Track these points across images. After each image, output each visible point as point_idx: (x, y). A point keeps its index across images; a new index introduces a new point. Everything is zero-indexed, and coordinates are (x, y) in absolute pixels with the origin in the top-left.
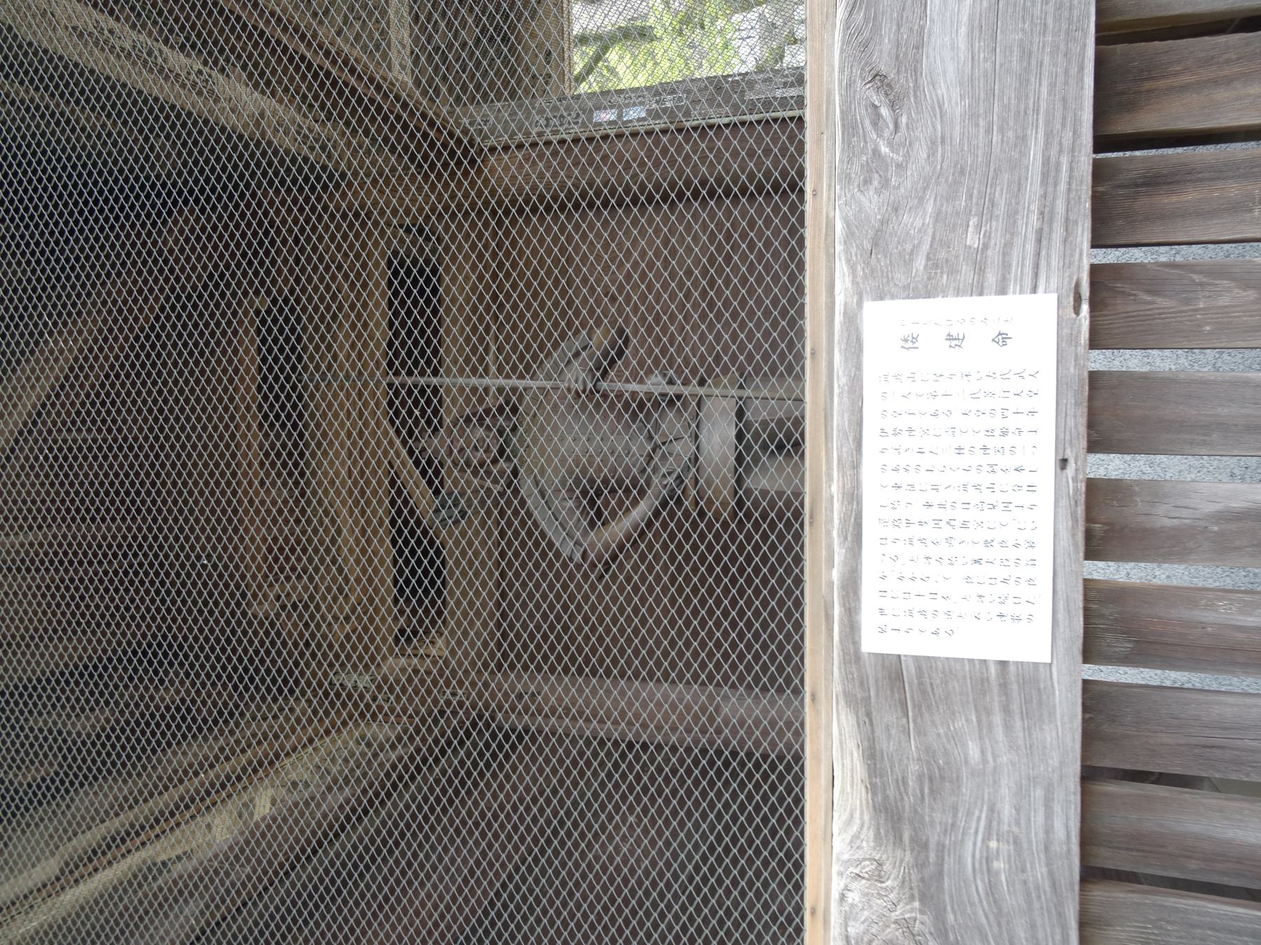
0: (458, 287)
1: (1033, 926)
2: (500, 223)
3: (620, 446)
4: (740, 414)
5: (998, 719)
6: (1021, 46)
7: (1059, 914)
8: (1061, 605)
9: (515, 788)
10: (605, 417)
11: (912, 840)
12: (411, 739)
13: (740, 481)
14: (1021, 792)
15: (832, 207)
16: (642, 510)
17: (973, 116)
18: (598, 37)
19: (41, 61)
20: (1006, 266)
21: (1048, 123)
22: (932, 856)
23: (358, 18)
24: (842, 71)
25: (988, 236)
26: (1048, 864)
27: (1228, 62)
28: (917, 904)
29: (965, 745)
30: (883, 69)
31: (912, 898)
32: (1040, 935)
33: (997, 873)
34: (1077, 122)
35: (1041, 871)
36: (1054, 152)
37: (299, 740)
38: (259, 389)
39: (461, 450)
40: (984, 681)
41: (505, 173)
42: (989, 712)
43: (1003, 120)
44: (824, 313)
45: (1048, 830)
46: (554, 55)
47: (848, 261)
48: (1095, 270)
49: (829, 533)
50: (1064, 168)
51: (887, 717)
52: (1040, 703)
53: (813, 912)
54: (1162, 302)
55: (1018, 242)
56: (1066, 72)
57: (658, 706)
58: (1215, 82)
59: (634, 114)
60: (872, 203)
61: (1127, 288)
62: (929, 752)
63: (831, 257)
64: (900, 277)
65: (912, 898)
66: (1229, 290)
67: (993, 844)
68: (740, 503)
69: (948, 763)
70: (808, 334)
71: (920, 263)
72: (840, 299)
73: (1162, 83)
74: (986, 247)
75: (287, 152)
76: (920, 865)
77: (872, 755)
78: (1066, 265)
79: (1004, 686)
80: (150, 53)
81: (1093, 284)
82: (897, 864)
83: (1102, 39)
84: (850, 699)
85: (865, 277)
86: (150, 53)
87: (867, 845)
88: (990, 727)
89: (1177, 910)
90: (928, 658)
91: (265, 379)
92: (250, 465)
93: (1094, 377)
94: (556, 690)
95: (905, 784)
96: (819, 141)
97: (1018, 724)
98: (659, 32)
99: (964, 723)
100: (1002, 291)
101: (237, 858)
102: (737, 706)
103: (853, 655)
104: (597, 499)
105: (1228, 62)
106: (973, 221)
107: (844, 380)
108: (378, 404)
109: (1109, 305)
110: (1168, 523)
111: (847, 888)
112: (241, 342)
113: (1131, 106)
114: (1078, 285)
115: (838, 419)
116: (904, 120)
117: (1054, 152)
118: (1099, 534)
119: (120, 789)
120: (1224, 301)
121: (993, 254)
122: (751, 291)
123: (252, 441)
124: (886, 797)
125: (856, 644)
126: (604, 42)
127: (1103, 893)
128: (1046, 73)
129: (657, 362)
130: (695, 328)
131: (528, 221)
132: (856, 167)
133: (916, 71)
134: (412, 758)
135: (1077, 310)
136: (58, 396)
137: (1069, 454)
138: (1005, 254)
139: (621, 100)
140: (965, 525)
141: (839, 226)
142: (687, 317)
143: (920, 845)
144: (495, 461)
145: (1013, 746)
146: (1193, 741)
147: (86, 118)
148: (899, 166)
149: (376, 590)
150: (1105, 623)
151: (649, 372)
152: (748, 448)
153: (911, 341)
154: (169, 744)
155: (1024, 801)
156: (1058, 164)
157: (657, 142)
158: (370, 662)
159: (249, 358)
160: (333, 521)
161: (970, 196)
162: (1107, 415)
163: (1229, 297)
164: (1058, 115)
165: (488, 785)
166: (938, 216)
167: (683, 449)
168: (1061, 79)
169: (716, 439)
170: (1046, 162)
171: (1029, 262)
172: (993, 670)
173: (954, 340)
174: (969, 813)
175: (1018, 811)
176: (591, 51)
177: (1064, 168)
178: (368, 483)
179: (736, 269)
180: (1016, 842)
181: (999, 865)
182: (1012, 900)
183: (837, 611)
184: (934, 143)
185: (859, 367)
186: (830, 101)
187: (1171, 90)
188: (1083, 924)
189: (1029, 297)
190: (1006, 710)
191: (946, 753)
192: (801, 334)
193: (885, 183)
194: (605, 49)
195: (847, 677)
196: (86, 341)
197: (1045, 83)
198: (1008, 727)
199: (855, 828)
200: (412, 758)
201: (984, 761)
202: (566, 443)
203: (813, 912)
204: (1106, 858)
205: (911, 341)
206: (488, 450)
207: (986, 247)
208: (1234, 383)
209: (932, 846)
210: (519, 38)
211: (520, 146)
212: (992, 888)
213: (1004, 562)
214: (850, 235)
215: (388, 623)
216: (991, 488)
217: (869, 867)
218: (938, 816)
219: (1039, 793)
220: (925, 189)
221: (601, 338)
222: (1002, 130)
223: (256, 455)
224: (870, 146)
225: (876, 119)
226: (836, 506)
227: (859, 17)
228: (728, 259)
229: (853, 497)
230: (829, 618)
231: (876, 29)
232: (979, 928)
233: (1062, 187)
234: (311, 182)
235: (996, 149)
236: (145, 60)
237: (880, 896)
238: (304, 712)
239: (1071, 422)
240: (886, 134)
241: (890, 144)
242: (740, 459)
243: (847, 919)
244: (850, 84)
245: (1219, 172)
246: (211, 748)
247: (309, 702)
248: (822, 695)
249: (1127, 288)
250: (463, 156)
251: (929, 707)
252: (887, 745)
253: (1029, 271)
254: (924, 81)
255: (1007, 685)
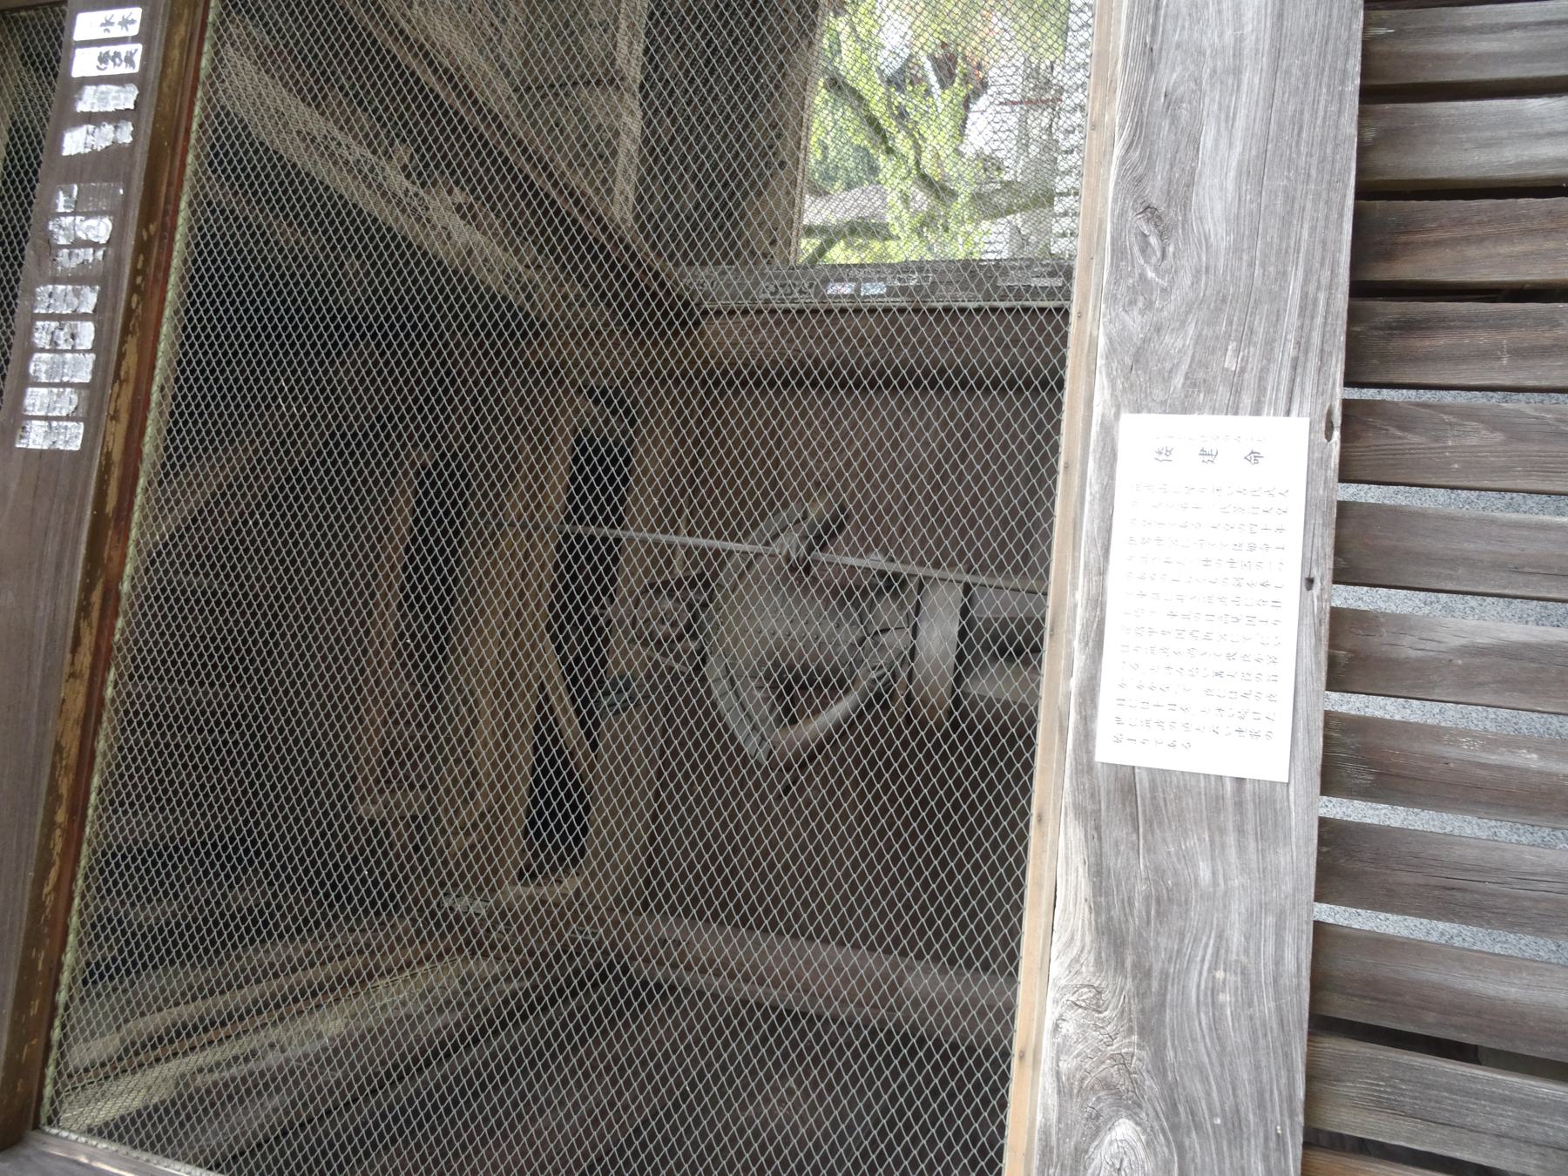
0: (652, 461)
1: (1258, 1067)
2: (708, 393)
3: (823, 633)
4: (964, 612)
5: (1231, 840)
6: (1286, 190)
7: (1286, 1055)
8: (1301, 724)
9: (646, 1041)
10: (812, 601)
11: (1134, 966)
12: (529, 974)
13: (959, 680)
14: (1252, 919)
15: (1090, 389)
16: (839, 709)
17: (1237, 250)
18: (823, 230)
19: (274, 167)
20: (1261, 390)
21: (1308, 262)
22: (1155, 985)
23: (582, 165)
24: (1115, 201)
25: (1245, 360)
26: (1277, 999)
27: (1480, 223)
28: (1135, 1038)
29: (1195, 866)
30: (1154, 202)
31: (1130, 1031)
32: (1265, 1077)
33: (1222, 1007)
34: (1335, 264)
35: (1269, 1006)
36: (1312, 288)
37: (396, 961)
38: (407, 549)
39: (647, 621)
40: (1219, 798)
41: (724, 340)
42: (1222, 831)
43: (1265, 255)
44: (1080, 425)
45: (1279, 961)
46: (784, 228)
47: (1109, 375)
48: (1347, 404)
49: (1069, 642)
50: (1321, 303)
51: (1117, 832)
52: (1276, 825)
53: (1022, 1057)
54: (1414, 439)
55: (1274, 367)
56: (1327, 218)
57: (829, 971)
58: (1467, 240)
59: (874, 289)
60: (1135, 322)
61: (1378, 423)
62: (1159, 871)
63: (1091, 373)
64: (1158, 393)
65: (1130, 1031)
66: (1476, 431)
67: (1220, 974)
68: (957, 702)
69: (1176, 884)
70: (1062, 449)
71: (1178, 381)
72: (1097, 411)
73: (1418, 237)
74: (1243, 370)
75: (488, 289)
76: (1142, 995)
77: (1098, 873)
78: (1320, 392)
79: (1239, 804)
80: (372, 170)
81: (1345, 416)
82: (1118, 991)
83: (1362, 193)
84: (1079, 811)
85: (1124, 390)
86: (372, 170)
87: (1087, 971)
88: (1223, 847)
89: (1412, 1068)
90: (1164, 771)
91: (414, 540)
92: (382, 644)
93: (1343, 507)
94: (708, 940)
95: (1131, 905)
96: (1087, 268)
97: (1252, 845)
98: (895, 230)
99: (1197, 842)
100: (1257, 411)
101: (329, 1060)
102: (926, 982)
103: (1085, 766)
104: (796, 688)
105: (1480, 223)
106: (1232, 346)
107: (1096, 488)
108: (541, 586)
109: (1360, 441)
110: (1413, 654)
111: (1061, 1018)
112: (396, 502)
113: (1388, 256)
114: (1330, 414)
115: (1089, 525)
116: (1171, 249)
117: (1312, 288)
118: (1344, 661)
119: (197, 976)
120: (1472, 441)
121: (1250, 378)
122: (983, 489)
123: (388, 620)
124: (1110, 919)
125: (1090, 753)
126: (830, 234)
127: (1336, 1046)
128: (1307, 217)
129: (877, 540)
130: (916, 531)
131: (736, 393)
132: (1123, 289)
133: (1186, 206)
134: (527, 995)
135: (1329, 437)
136: (182, 537)
137: (1316, 574)
138: (1262, 379)
139: (861, 274)
140: (1207, 637)
141: (1102, 342)
142: (909, 519)
143: (1143, 973)
144: (680, 637)
145: (1245, 869)
146: (1433, 881)
147: (284, 233)
148: (1164, 290)
149: (510, 799)
150: (1347, 758)
151: (868, 550)
152: (970, 646)
153: (1165, 454)
154: (252, 941)
155: (1255, 928)
156: (1316, 300)
157: (893, 321)
158: (486, 887)
159: (402, 519)
160: (470, 711)
161: (1230, 323)
162: (1356, 549)
163: (1479, 438)
164: (1318, 257)
165: (618, 1036)
166: (1198, 338)
167: (897, 640)
168: (1321, 224)
169: (936, 633)
170: (1305, 296)
171: (1284, 388)
172: (1229, 787)
173: (1207, 455)
174: (1196, 940)
175: (1247, 939)
176: (817, 242)
177: (1321, 303)
178: (519, 665)
179: (970, 467)
180: (1244, 973)
181: (1225, 998)
182: (1236, 1037)
183: (1073, 717)
184: (1198, 271)
185: (1112, 477)
186: (1101, 230)
187: (1425, 244)
188: (1309, 1079)
189: (1282, 420)
190: (1241, 831)
191: (1176, 872)
192: (1055, 449)
193: (1149, 305)
194: (830, 243)
195: (1077, 789)
196: (226, 477)
197: (1306, 226)
198: (1241, 849)
199: (1075, 951)
200: (527, 995)
201: (1215, 884)
202: (765, 622)
203: (1022, 1057)
204: (1342, 1008)
205: (1165, 454)
206: (674, 625)
207: (1243, 370)
208: (1480, 521)
209: (1155, 974)
210: (743, 215)
211: (745, 312)
212: (1216, 1023)
213: (1246, 677)
214: (1112, 351)
215: (514, 851)
216: (1236, 601)
217: (1087, 994)
218: (1163, 941)
219: (1270, 920)
220: (1187, 313)
221: (818, 509)
222: (1263, 265)
223: (390, 634)
224: (1137, 271)
225: (1145, 247)
226: (1080, 611)
227: (1135, 155)
228: (963, 457)
229: (1097, 603)
230: (1063, 730)
231: (1150, 166)
232: (1200, 1068)
233: (1319, 320)
234: (505, 326)
235: (1258, 282)
236: (367, 177)
237: (1097, 1028)
238: (406, 931)
239: (1318, 542)
240: (1154, 260)
241: (1156, 270)
242: (960, 657)
243: (1060, 1052)
244: (1123, 213)
245: (1469, 323)
246: (296, 949)
247: (414, 921)
248: (1049, 816)
249: (1378, 423)
250: (683, 316)
251: (1161, 823)
252: (1114, 862)
253: (1283, 395)
254: (1193, 216)
255: (1243, 803)
